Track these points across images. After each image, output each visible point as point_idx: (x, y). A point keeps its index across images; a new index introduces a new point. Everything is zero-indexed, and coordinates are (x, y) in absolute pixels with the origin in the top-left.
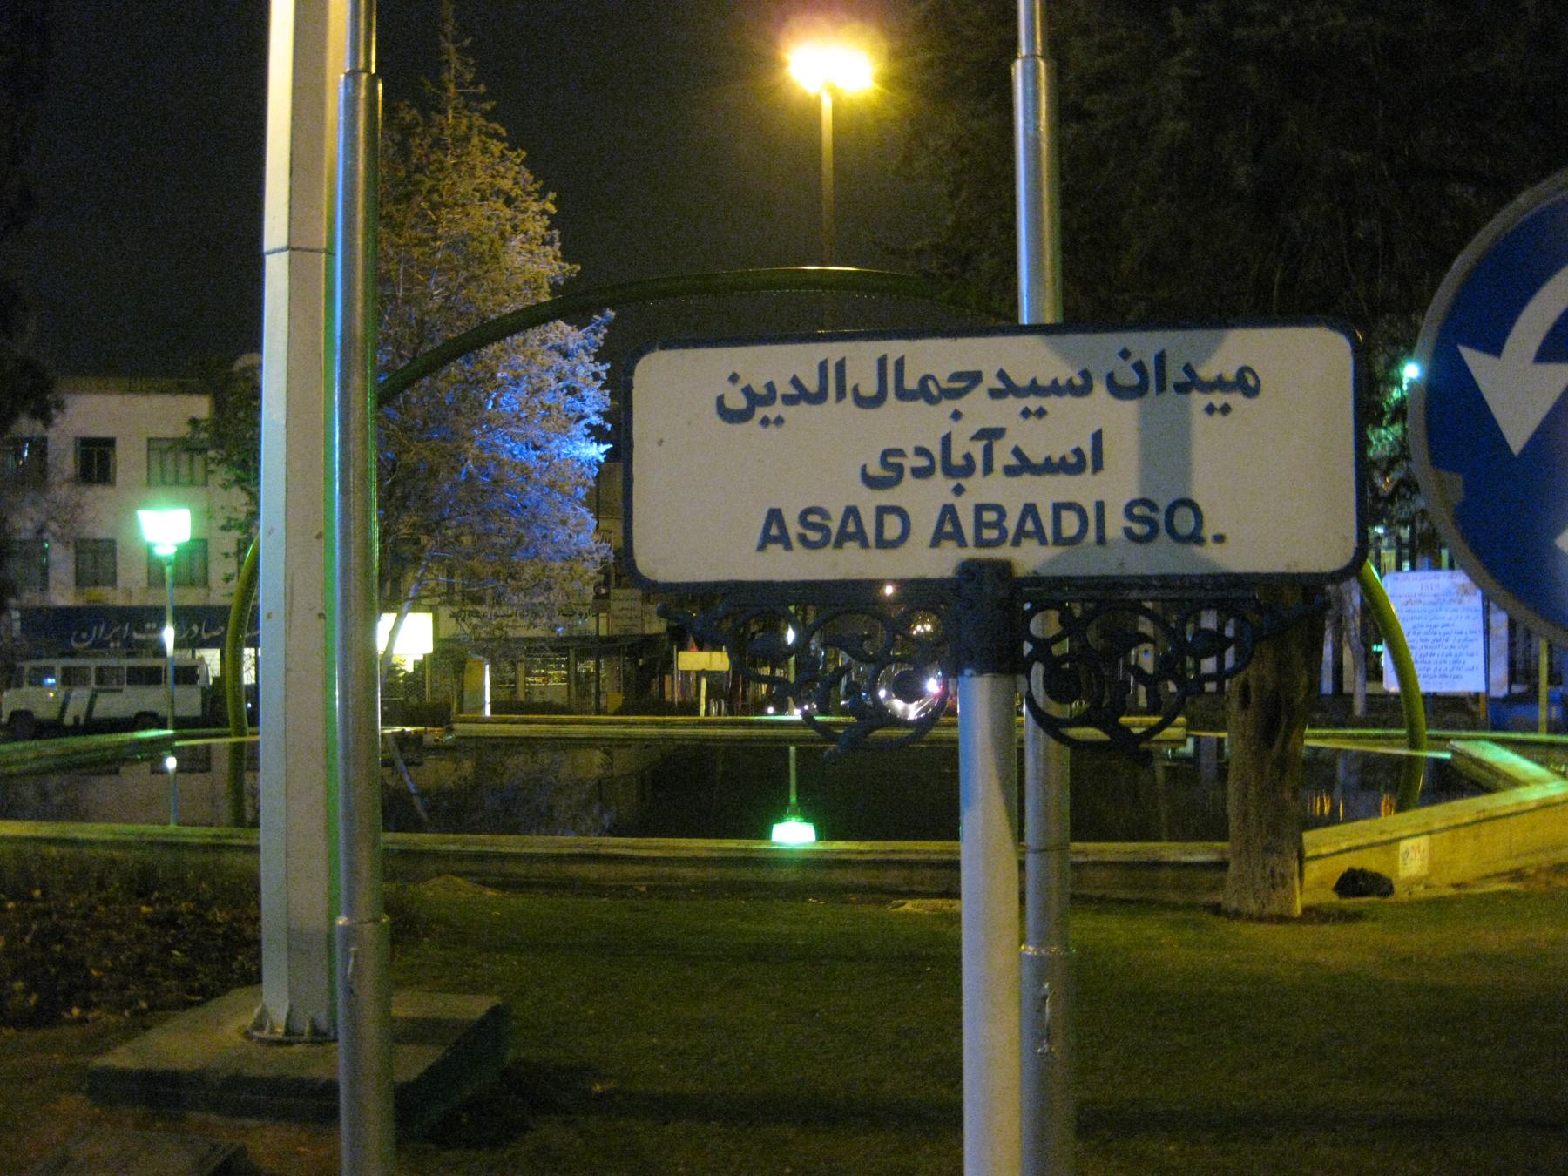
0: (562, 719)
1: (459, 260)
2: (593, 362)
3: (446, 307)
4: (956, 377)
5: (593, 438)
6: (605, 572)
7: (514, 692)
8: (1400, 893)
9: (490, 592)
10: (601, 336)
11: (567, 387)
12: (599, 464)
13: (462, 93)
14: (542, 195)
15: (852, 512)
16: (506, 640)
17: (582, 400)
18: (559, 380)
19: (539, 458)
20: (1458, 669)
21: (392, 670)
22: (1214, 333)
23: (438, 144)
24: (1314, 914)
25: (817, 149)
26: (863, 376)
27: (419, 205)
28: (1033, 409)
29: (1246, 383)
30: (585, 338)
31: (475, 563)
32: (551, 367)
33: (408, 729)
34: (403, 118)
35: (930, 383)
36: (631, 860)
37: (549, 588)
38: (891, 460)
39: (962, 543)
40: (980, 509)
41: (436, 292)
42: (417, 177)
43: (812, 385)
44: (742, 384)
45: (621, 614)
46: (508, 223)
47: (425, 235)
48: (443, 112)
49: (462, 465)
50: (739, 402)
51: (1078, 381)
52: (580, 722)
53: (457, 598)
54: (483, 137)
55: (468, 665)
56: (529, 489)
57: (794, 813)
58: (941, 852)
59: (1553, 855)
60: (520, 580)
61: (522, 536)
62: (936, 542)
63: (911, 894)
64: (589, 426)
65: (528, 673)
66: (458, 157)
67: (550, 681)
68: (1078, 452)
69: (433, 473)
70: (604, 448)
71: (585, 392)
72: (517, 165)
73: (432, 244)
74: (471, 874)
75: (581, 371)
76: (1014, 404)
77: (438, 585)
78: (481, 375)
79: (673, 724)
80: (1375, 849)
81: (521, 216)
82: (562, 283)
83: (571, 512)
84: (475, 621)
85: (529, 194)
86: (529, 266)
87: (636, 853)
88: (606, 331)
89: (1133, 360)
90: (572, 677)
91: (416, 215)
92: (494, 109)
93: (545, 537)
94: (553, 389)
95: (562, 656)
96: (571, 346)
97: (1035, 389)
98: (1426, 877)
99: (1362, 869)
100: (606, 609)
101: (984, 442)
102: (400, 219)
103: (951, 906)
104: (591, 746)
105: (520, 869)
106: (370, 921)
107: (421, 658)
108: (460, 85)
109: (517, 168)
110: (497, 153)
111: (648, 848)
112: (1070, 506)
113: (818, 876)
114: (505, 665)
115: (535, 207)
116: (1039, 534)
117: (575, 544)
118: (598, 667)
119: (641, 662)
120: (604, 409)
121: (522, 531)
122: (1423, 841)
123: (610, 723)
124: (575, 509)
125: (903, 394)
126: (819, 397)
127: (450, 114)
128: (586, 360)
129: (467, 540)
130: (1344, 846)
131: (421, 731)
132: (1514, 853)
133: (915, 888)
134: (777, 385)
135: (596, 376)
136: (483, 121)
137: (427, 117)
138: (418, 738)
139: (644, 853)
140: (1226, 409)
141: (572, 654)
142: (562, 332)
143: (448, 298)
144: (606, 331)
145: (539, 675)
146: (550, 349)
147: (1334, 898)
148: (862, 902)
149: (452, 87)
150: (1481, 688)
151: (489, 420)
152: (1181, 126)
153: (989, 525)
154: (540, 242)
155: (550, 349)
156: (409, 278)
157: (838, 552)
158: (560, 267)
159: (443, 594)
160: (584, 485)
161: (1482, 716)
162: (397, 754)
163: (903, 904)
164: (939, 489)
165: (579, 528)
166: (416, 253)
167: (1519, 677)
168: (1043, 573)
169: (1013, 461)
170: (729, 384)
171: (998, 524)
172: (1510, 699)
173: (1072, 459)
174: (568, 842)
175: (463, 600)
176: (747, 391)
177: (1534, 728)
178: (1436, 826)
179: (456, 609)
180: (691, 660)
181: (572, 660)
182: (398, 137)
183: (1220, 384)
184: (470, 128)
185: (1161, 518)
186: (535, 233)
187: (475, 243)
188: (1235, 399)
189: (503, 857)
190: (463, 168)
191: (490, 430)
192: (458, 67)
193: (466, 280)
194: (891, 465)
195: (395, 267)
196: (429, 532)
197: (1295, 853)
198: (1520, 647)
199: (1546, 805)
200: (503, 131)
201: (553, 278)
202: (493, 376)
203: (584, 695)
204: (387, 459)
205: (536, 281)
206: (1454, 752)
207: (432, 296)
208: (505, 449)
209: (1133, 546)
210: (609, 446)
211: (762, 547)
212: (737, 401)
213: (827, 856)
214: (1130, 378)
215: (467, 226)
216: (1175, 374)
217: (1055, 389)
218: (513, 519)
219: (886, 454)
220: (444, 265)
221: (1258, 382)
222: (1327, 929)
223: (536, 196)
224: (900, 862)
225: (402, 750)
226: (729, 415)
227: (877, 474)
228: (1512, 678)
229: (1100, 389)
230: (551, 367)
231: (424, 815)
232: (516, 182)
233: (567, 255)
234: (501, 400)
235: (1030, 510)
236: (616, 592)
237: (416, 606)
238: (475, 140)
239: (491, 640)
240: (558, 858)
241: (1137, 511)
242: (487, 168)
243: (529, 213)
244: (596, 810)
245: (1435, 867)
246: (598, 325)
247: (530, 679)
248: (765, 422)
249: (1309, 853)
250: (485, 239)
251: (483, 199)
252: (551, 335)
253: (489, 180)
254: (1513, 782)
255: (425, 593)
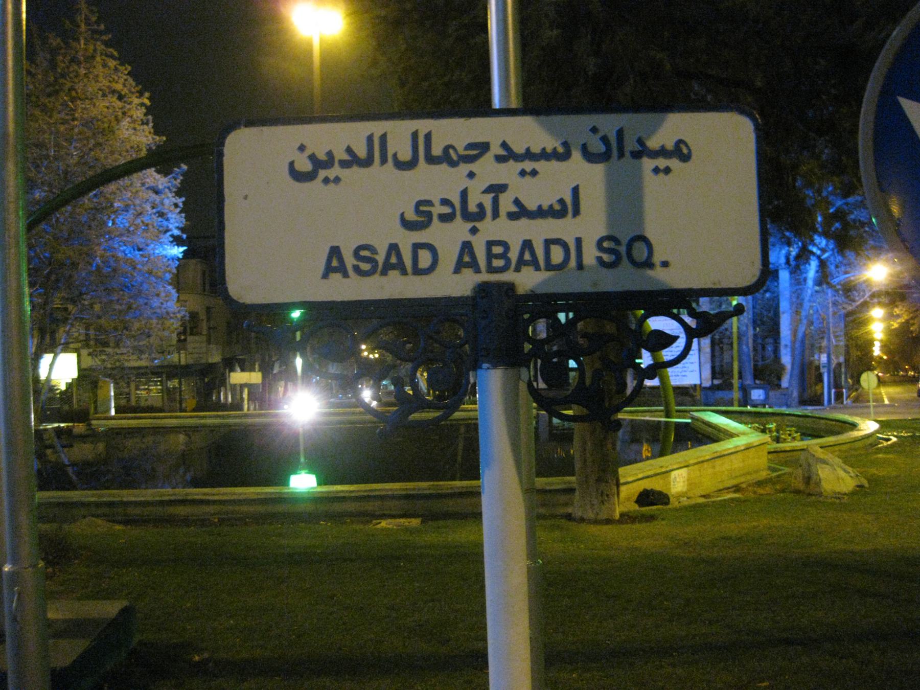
0: (159, 416)
1: (89, 133)
2: (174, 197)
3: (82, 162)
4: (470, 146)
5: (175, 243)
6: (183, 325)
7: (129, 400)
8: (674, 503)
9: (112, 339)
10: (179, 181)
11: (158, 212)
12: (179, 259)
13: (89, 30)
14: (141, 94)
15: (394, 248)
16: (123, 369)
17: (167, 220)
18: (153, 208)
19: (142, 255)
20: (685, 371)
21: (52, 389)
22: (661, 115)
23: (73, 60)
24: (627, 518)
25: (312, 63)
26: (401, 147)
27: (63, 99)
28: (528, 170)
29: (681, 152)
30: (169, 182)
31: (102, 321)
32: (148, 200)
33: (62, 425)
34: (51, 44)
35: (451, 151)
36: (208, 502)
37: (149, 336)
38: (422, 208)
39: (478, 271)
40: (490, 244)
41: (75, 153)
42: (61, 81)
43: (362, 152)
44: (308, 152)
45: (194, 351)
46: (121, 111)
47: (67, 117)
48: (78, 40)
49: (94, 260)
50: (307, 167)
51: (561, 150)
52: (171, 417)
53: (92, 343)
54: (104, 57)
55: (100, 384)
56: (135, 275)
57: (303, 469)
58: (400, 489)
59: (754, 476)
60: (131, 331)
61: (132, 303)
62: (457, 270)
63: (383, 516)
64: (172, 236)
65: (137, 388)
66: (88, 69)
67: (151, 392)
68: (561, 201)
69: (74, 265)
70: (182, 249)
71: (170, 215)
72: (125, 74)
73: (72, 123)
74: (105, 515)
75: (167, 202)
76: (514, 167)
77: (79, 335)
78: (104, 205)
79: (229, 417)
80: (658, 477)
81: (128, 107)
82: (154, 148)
83: (162, 289)
84: (104, 357)
85: (133, 93)
86: (133, 137)
87: (211, 498)
88: (181, 178)
89: (601, 134)
90: (165, 391)
91: (62, 105)
92: (110, 39)
93: (146, 304)
94: (150, 213)
95: (158, 377)
96: (160, 187)
97: (529, 155)
98: (686, 493)
99: (652, 489)
100: (185, 349)
101: (492, 195)
102: (50, 106)
103: (409, 523)
104: (177, 432)
105: (138, 511)
106: (29, 567)
107: (70, 381)
108: (88, 23)
109: (125, 77)
110: (113, 67)
111: (218, 495)
112: (557, 242)
113: (322, 508)
114: (123, 384)
115: (137, 101)
116: (535, 263)
117: (165, 308)
118: (180, 383)
119: (206, 380)
120: (181, 225)
121: (131, 301)
122: (684, 472)
123: (191, 417)
124: (164, 287)
125: (431, 160)
126: (367, 162)
127: (82, 42)
128: (170, 195)
129: (97, 307)
130: (640, 476)
131: (71, 426)
132: (733, 476)
133: (385, 512)
134: (335, 153)
135: (176, 205)
136: (103, 47)
137: (67, 44)
138: (69, 431)
139: (216, 498)
140: (667, 170)
141: (164, 376)
142: (155, 179)
143: (82, 157)
144: (181, 178)
145: (145, 389)
146: (148, 188)
147: (636, 507)
148: (352, 522)
149: (83, 26)
150: (698, 382)
151: (109, 233)
152: (555, 32)
153: (497, 256)
154: (140, 123)
155: (148, 188)
156: (57, 145)
157: (383, 279)
158: (153, 139)
159: (82, 341)
160: (170, 272)
161: (698, 397)
162: (56, 440)
163: (380, 523)
164: (460, 230)
165: (167, 299)
166: (62, 128)
167: (717, 376)
168: (539, 291)
169: (514, 209)
170: (298, 153)
171: (504, 256)
172: (713, 388)
173: (557, 207)
174: (167, 493)
175: (96, 344)
176: (312, 158)
177: (731, 404)
178: (691, 462)
179: (91, 350)
180: (238, 377)
181: (164, 378)
182: (48, 56)
183: (663, 152)
184: (95, 50)
185: (623, 249)
186: (137, 117)
187: (99, 123)
188: (674, 163)
189: (127, 504)
190: (91, 76)
191: (111, 239)
192: (87, 13)
193: (94, 145)
194: (424, 212)
195: (48, 137)
196: (73, 301)
197: (615, 482)
198: (717, 360)
199: (748, 448)
200: (116, 53)
201: (148, 145)
202: (112, 206)
203: (172, 400)
204: (45, 257)
205: (138, 147)
206: (692, 418)
207: (73, 155)
208: (120, 250)
209: (605, 270)
210: (185, 248)
211: (325, 276)
212: (304, 165)
213: (330, 495)
214: (598, 147)
215: (94, 112)
216: (630, 145)
217: (544, 155)
218: (125, 293)
219: (419, 204)
220: (79, 136)
221: (690, 150)
222: (637, 526)
223: (138, 94)
224: (375, 497)
225: (59, 437)
226: (297, 176)
227: (411, 219)
228: (714, 375)
229: (576, 155)
230: (148, 200)
231: (74, 477)
232: (124, 85)
233: (157, 131)
234: (117, 221)
235: (527, 245)
236: (190, 338)
237: (66, 349)
238: (98, 59)
239: (113, 369)
240: (162, 503)
241: (605, 244)
242: (107, 76)
243: (133, 105)
244: (181, 471)
245: (691, 484)
246: (177, 174)
247: (138, 392)
248: (326, 181)
249: (622, 481)
250: (105, 120)
251: (104, 95)
252: (148, 180)
253: (108, 84)
254: (730, 435)
255: (71, 340)
